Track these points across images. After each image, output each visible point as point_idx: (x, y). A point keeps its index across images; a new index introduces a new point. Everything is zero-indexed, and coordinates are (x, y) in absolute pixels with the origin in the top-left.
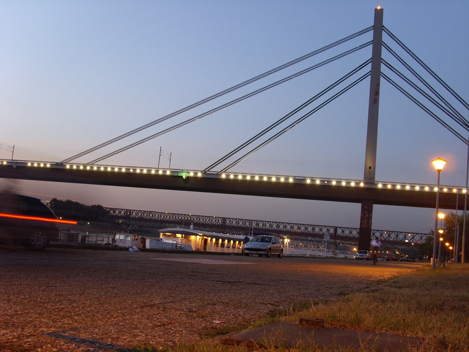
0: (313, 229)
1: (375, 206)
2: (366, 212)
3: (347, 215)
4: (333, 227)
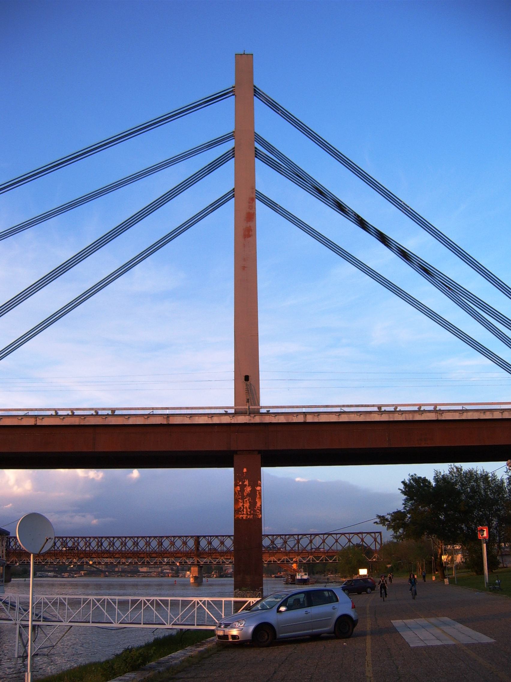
0: (160, 544)
1: (266, 471)
2: (246, 483)
3: (202, 493)
4: (192, 537)
